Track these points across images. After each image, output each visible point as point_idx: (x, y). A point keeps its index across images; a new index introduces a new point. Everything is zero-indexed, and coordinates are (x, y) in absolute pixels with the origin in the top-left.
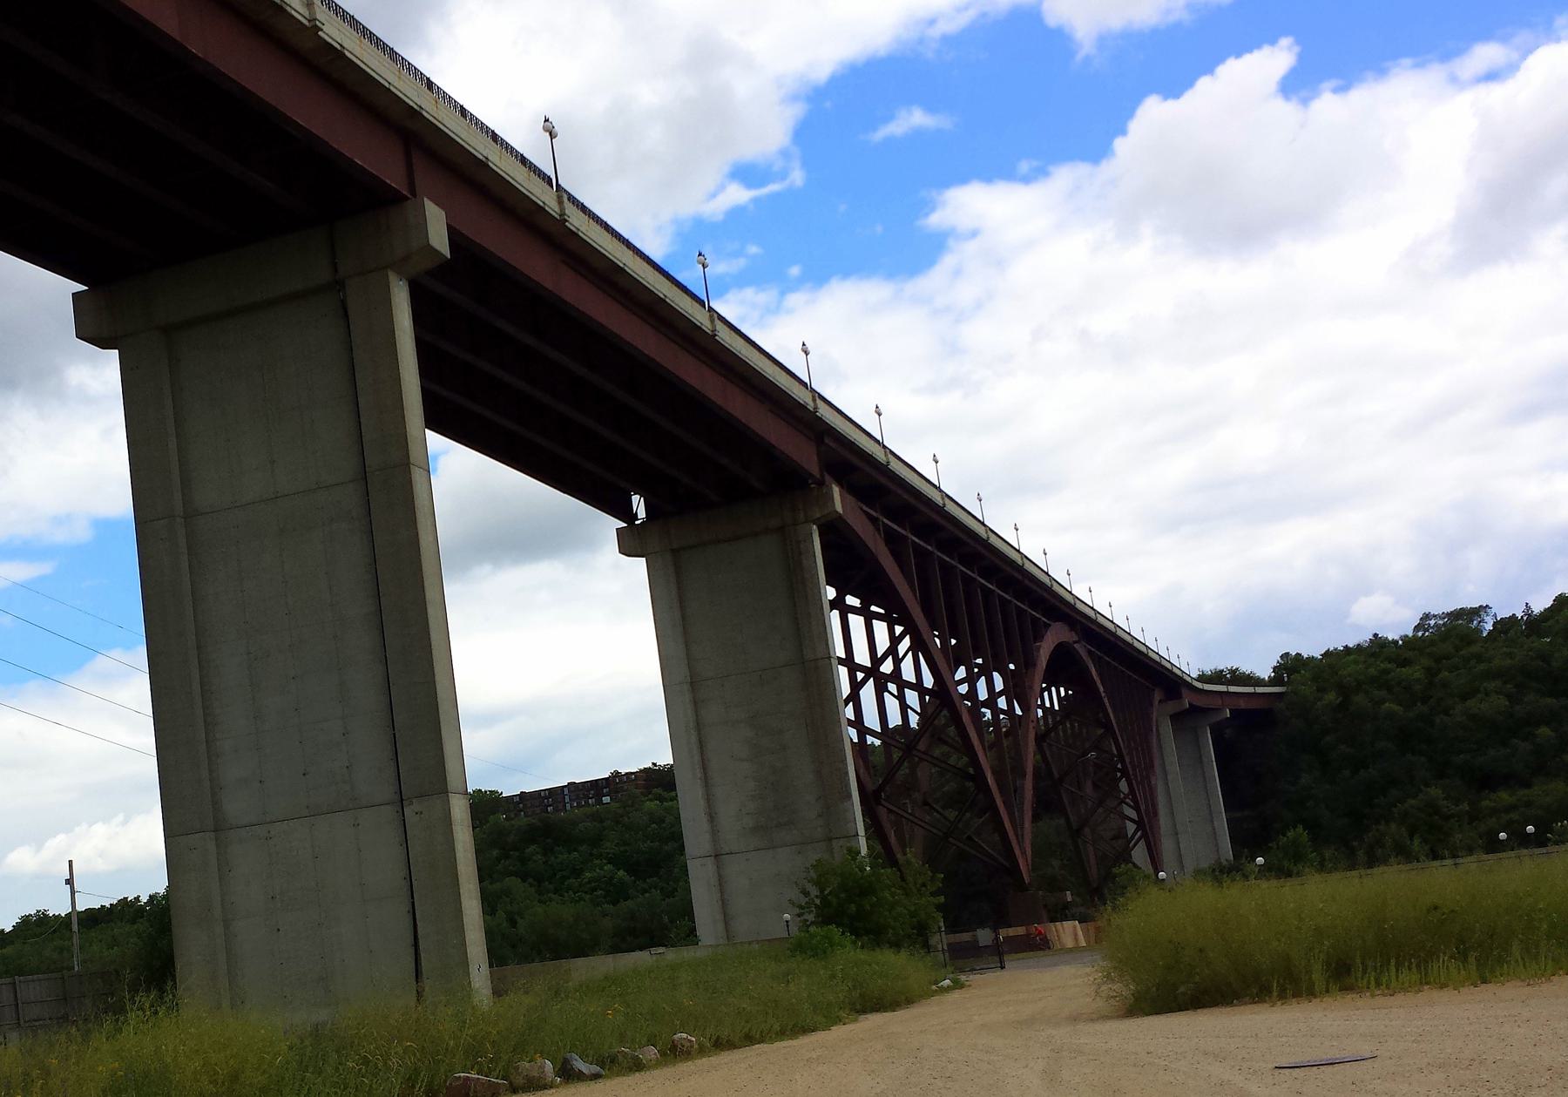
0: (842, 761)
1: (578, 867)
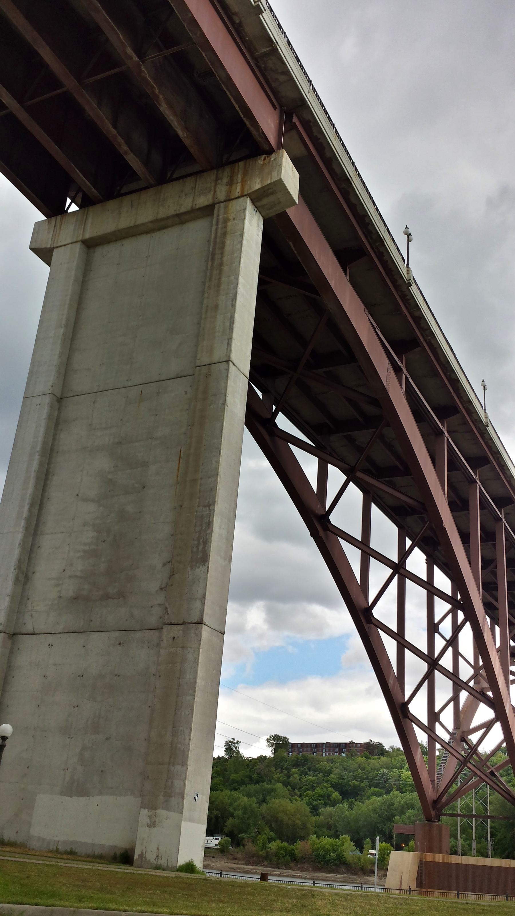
0: (209, 506)
1: (315, 785)
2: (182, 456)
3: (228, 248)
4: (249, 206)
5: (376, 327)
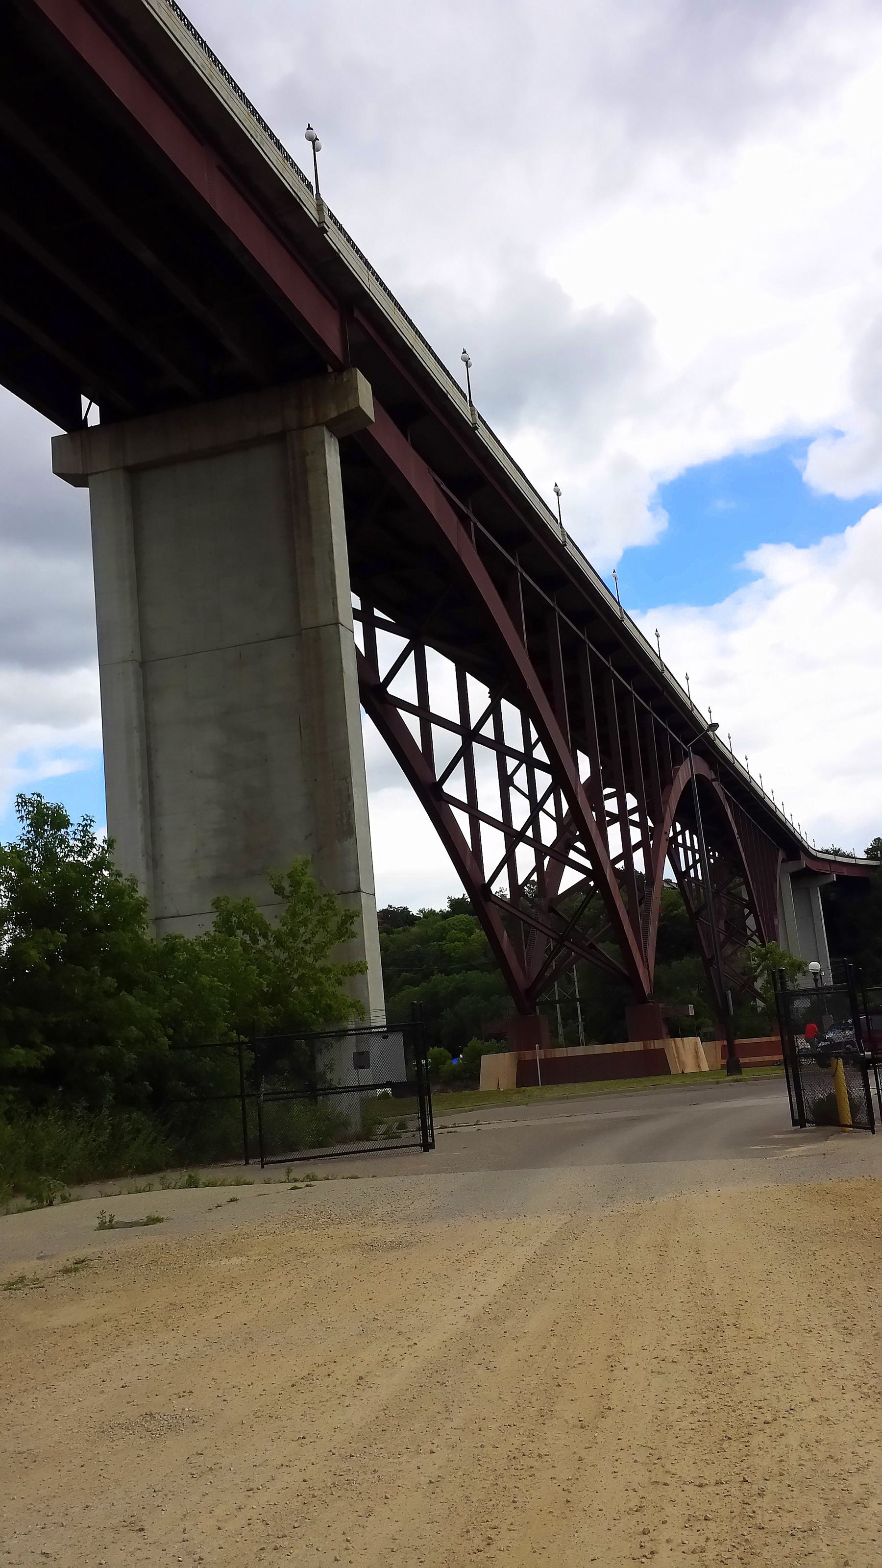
0: (346, 779)
2: (301, 725)
4: (327, 434)
5: (440, 483)
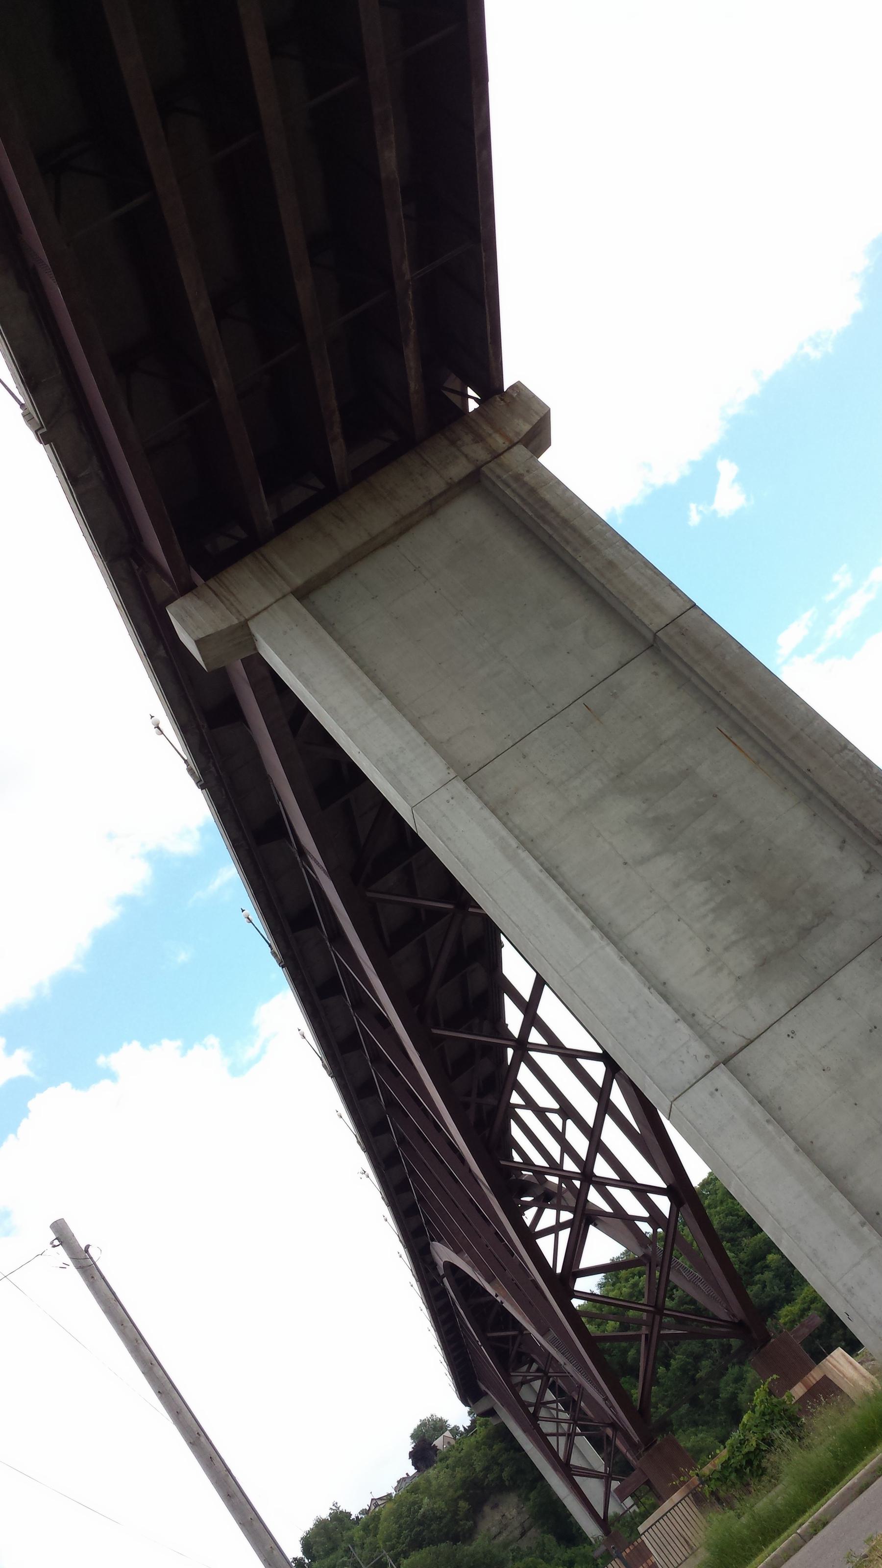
3: (555, 503)
